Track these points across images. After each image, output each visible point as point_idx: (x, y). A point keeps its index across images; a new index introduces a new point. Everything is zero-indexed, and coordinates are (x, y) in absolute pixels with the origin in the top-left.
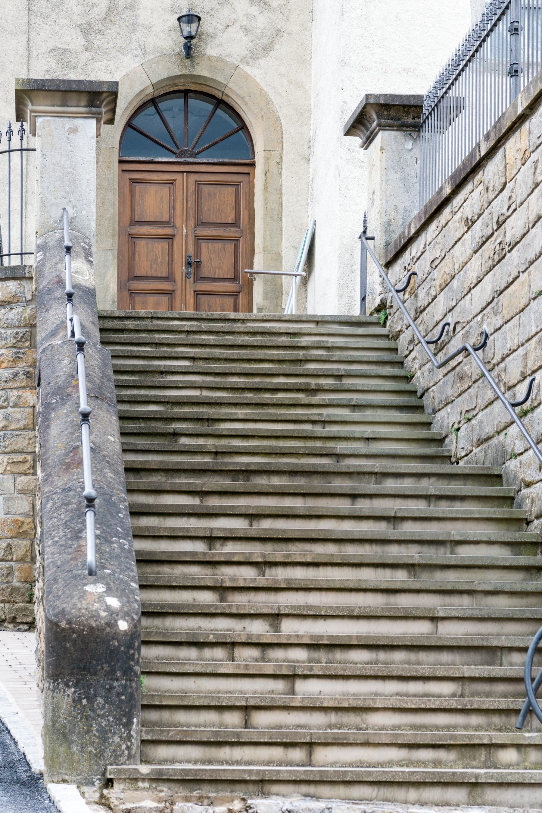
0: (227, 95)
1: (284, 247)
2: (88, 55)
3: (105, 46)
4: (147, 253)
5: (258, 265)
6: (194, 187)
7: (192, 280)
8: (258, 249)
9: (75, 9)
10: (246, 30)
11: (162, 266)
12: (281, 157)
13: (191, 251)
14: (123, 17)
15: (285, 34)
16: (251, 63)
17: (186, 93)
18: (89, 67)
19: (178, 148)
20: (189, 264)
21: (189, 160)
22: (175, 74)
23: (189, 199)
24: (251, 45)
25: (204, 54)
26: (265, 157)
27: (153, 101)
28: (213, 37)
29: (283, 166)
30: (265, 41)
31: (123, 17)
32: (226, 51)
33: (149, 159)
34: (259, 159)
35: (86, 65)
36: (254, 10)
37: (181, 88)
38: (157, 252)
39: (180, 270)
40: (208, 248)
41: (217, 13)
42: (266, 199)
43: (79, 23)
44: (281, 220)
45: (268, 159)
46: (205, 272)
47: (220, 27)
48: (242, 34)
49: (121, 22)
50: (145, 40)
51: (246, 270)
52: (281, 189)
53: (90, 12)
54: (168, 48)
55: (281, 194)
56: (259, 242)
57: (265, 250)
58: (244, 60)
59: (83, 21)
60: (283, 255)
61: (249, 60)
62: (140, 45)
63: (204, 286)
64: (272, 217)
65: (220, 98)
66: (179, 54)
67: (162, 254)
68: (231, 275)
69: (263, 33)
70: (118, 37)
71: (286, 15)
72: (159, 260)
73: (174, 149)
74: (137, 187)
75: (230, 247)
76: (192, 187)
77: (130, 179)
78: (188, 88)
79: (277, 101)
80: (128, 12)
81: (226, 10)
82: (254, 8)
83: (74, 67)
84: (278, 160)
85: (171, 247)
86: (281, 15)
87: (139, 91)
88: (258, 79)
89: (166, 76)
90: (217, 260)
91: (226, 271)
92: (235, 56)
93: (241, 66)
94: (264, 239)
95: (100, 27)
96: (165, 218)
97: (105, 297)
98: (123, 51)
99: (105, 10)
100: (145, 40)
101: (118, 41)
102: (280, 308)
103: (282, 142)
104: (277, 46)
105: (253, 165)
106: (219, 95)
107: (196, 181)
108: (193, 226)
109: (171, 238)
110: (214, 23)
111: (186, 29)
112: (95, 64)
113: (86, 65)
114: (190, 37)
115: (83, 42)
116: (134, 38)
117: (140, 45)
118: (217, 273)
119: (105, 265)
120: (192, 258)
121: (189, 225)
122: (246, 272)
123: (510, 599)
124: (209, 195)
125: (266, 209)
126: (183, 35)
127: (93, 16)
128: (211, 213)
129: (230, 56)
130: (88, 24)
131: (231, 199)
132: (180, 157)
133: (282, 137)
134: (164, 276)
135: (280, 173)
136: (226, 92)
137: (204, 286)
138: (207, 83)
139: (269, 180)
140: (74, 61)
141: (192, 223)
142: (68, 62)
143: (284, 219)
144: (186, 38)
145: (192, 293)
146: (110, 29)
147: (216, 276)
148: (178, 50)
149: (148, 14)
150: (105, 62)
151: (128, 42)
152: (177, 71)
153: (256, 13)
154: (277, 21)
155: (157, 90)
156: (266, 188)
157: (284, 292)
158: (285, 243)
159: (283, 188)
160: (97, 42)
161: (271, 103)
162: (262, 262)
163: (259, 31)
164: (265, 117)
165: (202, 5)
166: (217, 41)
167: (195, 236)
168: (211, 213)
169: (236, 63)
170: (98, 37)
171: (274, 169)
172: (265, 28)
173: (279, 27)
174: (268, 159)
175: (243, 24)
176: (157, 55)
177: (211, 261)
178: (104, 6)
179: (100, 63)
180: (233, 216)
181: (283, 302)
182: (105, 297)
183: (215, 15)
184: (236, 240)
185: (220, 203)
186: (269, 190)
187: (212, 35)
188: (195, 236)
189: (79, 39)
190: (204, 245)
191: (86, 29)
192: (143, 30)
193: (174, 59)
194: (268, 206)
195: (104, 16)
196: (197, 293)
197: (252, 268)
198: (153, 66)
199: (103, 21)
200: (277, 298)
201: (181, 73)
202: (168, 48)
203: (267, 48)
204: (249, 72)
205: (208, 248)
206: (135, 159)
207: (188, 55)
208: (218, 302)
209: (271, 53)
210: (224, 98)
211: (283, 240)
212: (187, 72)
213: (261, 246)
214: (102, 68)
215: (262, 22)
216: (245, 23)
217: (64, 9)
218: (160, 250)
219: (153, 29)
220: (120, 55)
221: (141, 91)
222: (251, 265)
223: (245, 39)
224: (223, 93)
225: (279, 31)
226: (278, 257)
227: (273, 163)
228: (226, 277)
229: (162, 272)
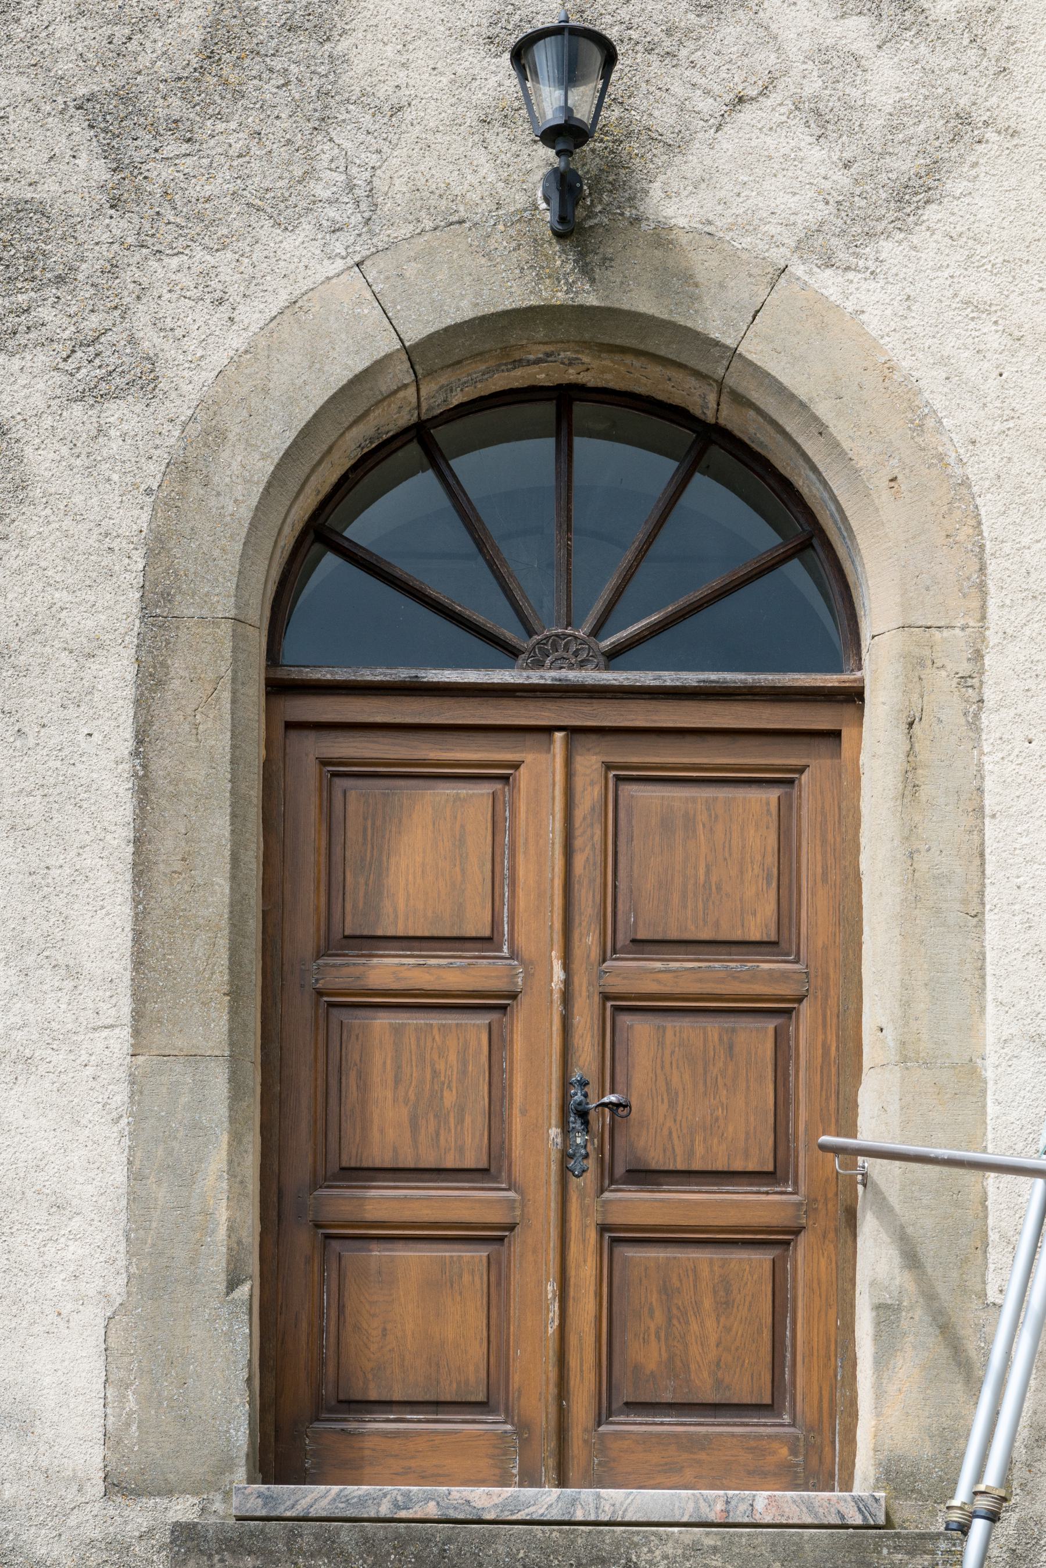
0: (740, 400)
1: (990, 1039)
2: (121, 226)
3: (198, 189)
4: (398, 1068)
5: (877, 1117)
6: (597, 791)
7: (589, 1180)
8: (875, 1049)
9: (63, 32)
10: (820, 120)
11: (461, 1121)
12: (978, 656)
13: (586, 1059)
14: (277, 64)
15: (990, 135)
16: (842, 256)
17: (562, 408)
18: (127, 276)
19: (530, 632)
20: (576, 1114)
21: (574, 676)
22: (508, 305)
23: (578, 843)
24: (843, 179)
25: (636, 221)
26: (905, 656)
27: (425, 441)
28: (677, 145)
29: (988, 694)
30: (904, 164)
31: (277, 64)
32: (733, 198)
33: (403, 674)
34: (880, 669)
35: (113, 268)
36: (856, 32)
37: (541, 376)
38: (441, 1066)
39: (538, 1137)
40: (661, 1043)
41: (691, 45)
42: (909, 833)
43: (81, 91)
44: (981, 923)
45: (917, 665)
46: (653, 1142)
47: (706, 105)
48: (802, 136)
49: (269, 87)
50: (374, 159)
51: (825, 1139)
52: (980, 790)
53: (132, 46)
54: (475, 197)
55: (979, 811)
56: (883, 1021)
57: (907, 1056)
58: (811, 244)
59: (102, 82)
60: (990, 1074)
61: (834, 241)
62: (351, 187)
63: (638, 1205)
64: (938, 911)
65: (710, 419)
66: (525, 216)
67: (464, 1072)
68: (760, 1160)
69: (893, 129)
70: (255, 150)
71: (993, 51)
72: (449, 1098)
73: (511, 634)
74: (352, 795)
75: (757, 1037)
76: (590, 793)
77: (324, 762)
78: (572, 375)
79: (957, 418)
80: (301, 45)
81: (732, 32)
82: (852, 22)
83: (60, 280)
84: (965, 668)
85: (498, 1043)
86: (973, 53)
87: (347, 376)
88: (873, 323)
89: (469, 314)
90: (691, 1094)
91: (743, 1142)
92: (772, 229)
93: (798, 269)
94: (906, 1004)
95: (176, 106)
96: (477, 924)
97: (193, 1261)
98: (280, 210)
99: (198, 35)
100: (374, 159)
101: (255, 165)
102: (975, 1304)
103: (982, 588)
104: (955, 186)
105: (853, 697)
106: (701, 401)
107: (608, 767)
108: (595, 953)
109: (497, 1004)
110: (677, 89)
111: (550, 101)
112: (153, 263)
113: (113, 268)
114: (566, 135)
115: (101, 171)
116: (325, 151)
117: (351, 187)
118: (699, 1150)
119: (196, 1125)
120: (592, 1090)
121: (578, 952)
122: (824, 1148)
123: (278, 438)
124: (666, 825)
125: (911, 878)
126: (533, 119)
127: (144, 60)
128: (676, 899)
129: (750, 228)
130: (124, 96)
131: (761, 841)
132: (539, 664)
133: (982, 569)
134: (469, 1163)
135: (974, 725)
136: (731, 381)
137: (638, 1205)
138: (651, 345)
139: (924, 754)
140: (60, 254)
141: (587, 941)
142: (30, 256)
143: (990, 919)
144: (551, 136)
145: (592, 1235)
146: (219, 116)
147: (696, 1166)
148: (521, 200)
149: (390, 51)
150: (199, 253)
151: (298, 172)
152: (514, 293)
153: (864, 47)
154: (955, 78)
155: (430, 373)
156: (910, 785)
157: (993, 1236)
158: (995, 1025)
159: (988, 784)
160: (161, 173)
161: (930, 423)
162: (894, 1107)
163: (875, 122)
164: (903, 484)
165: (624, 13)
166: (696, 159)
167: (606, 997)
168: (676, 899)
169: (778, 256)
170: (168, 151)
171: (945, 703)
172: (903, 108)
173: (963, 101)
174: (921, 663)
175: (808, 91)
176: (428, 224)
177: (673, 1103)
178: (190, 25)
179: (175, 262)
180: (768, 909)
181: (990, 1276)
182: (193, 1261)
183: (684, 53)
184: (782, 1011)
185: (706, 847)
186: (923, 794)
187: (669, 138)
188: (606, 997)
189: (82, 162)
190: (641, 1030)
191: (111, 118)
192: (367, 120)
193: (499, 242)
194: (922, 866)
195: (195, 63)
196: (615, 1237)
197: (853, 1133)
198: (411, 270)
199: (187, 84)
200: (966, 1260)
201: (534, 301)
202: (475, 197)
203: (914, 195)
204: (833, 293)
205: (661, 1043)
206: (342, 675)
207: (569, 228)
208: (705, 1272)
209: (931, 213)
210: (730, 417)
211: (991, 1009)
212: (560, 298)
213: (890, 1035)
214: (185, 280)
215: (887, 80)
216: (813, 86)
217: (18, 32)
218: (453, 1057)
219: (408, 115)
220: (265, 229)
221: (358, 380)
222: (846, 1118)
223: (816, 154)
224: (720, 384)
225: (964, 119)
226: (968, 1081)
227: (942, 681)
228: (738, 1166)
229: (461, 1150)
